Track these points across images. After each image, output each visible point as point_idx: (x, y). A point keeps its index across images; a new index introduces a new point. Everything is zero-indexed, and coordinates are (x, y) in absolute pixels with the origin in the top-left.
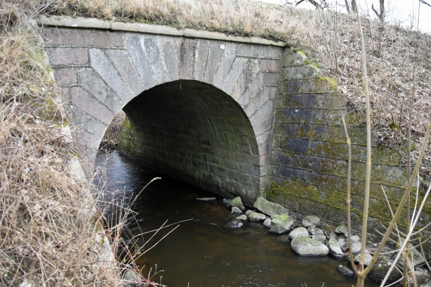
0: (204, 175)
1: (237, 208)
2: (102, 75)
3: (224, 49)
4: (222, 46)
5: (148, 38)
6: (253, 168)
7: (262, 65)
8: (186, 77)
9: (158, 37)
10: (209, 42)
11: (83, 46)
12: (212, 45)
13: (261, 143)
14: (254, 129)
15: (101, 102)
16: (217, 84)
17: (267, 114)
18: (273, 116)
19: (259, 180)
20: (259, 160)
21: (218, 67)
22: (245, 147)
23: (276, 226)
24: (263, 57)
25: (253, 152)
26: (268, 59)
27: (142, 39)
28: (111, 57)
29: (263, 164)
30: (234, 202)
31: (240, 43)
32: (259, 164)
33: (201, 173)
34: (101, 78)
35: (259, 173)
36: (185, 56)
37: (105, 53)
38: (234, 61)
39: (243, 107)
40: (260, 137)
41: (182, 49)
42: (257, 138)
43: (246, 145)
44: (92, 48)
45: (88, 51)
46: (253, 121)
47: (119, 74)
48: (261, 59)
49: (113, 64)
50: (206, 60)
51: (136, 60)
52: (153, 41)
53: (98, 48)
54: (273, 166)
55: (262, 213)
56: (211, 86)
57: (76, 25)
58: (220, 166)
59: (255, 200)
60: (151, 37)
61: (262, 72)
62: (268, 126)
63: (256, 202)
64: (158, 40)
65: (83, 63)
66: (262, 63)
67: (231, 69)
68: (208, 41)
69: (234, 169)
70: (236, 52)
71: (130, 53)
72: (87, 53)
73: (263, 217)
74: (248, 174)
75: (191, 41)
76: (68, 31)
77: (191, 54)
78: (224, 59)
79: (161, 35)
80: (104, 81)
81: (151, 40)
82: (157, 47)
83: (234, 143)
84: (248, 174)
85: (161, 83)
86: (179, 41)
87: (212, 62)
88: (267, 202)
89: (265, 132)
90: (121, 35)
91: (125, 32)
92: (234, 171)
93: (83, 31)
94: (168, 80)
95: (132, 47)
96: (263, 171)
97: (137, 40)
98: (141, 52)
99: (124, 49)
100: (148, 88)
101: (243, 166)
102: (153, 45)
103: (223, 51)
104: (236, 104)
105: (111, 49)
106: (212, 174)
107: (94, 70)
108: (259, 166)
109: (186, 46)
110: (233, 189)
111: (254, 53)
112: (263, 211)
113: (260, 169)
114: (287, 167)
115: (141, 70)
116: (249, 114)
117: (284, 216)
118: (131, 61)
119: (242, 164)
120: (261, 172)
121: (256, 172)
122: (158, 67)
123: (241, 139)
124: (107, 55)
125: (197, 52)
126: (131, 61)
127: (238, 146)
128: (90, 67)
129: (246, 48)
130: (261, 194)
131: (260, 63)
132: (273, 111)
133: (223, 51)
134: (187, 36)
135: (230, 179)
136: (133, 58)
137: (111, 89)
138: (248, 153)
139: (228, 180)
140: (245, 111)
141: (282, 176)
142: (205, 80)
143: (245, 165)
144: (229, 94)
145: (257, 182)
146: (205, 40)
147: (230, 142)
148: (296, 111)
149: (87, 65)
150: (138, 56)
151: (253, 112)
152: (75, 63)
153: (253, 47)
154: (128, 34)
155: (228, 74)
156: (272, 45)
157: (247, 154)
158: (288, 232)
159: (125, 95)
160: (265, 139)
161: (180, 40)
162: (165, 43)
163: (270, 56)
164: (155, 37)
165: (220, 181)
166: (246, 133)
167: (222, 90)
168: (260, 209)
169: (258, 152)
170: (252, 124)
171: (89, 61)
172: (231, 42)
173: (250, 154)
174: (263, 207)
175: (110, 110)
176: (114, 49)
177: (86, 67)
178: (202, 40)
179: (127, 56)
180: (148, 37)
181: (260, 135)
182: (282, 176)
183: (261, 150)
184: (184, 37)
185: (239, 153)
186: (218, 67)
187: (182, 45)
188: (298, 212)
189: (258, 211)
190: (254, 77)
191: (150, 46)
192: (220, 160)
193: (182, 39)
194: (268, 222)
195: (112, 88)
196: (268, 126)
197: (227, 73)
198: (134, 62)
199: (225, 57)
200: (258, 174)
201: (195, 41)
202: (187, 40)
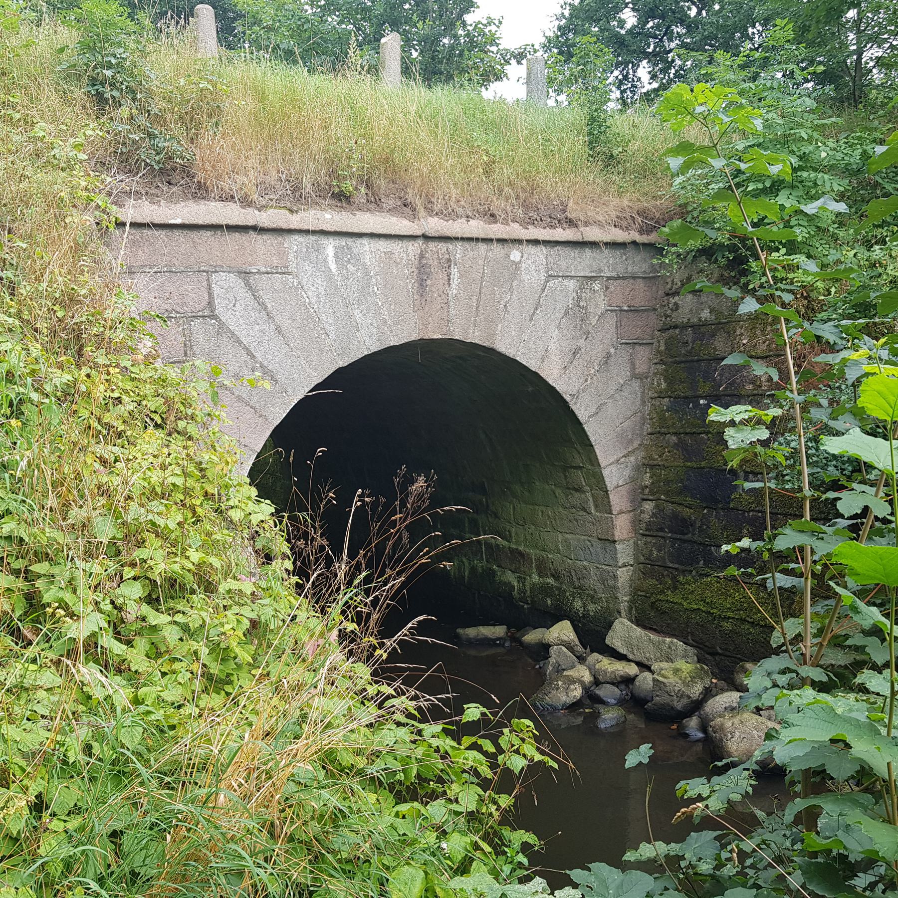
0: (473, 570)
1: (564, 649)
2: (241, 334)
3: (520, 262)
4: (515, 255)
5: (344, 243)
6: (598, 545)
7: (612, 293)
8: (434, 332)
9: (365, 241)
10: (483, 247)
11: (196, 268)
12: (490, 254)
13: (615, 483)
14: (597, 451)
15: (239, 399)
16: (503, 347)
17: (629, 413)
18: (643, 418)
19: (615, 577)
20: (613, 527)
21: (505, 306)
22: (577, 495)
23: (668, 689)
24: (614, 274)
25: (596, 506)
26: (624, 278)
27: (330, 246)
28: (261, 293)
29: (625, 536)
30: (556, 635)
31: (557, 243)
32: (613, 535)
33: (467, 564)
34: (240, 342)
35: (615, 559)
36: (429, 282)
37: (247, 284)
38: (543, 290)
39: (568, 398)
40: (614, 468)
41: (422, 272)
42: (606, 473)
43: (576, 490)
44: (216, 272)
45: (208, 280)
46: (592, 430)
47: (279, 330)
48: (609, 278)
49: (266, 308)
50: (478, 290)
51: (318, 296)
52: (355, 251)
53: (229, 272)
54: (649, 539)
55: (629, 660)
56: (491, 351)
57: (178, 221)
58: (514, 546)
59: (609, 625)
60: (349, 241)
61: (612, 311)
62: (631, 442)
63: (610, 633)
64: (367, 248)
65: (198, 307)
66: (612, 288)
67: (536, 309)
68: (480, 244)
69: (550, 551)
70: (548, 269)
71: (304, 282)
72: (205, 284)
73: (632, 669)
74: (585, 563)
75: (442, 246)
76: (162, 234)
77: (442, 276)
78: (519, 285)
79: (372, 235)
80: (246, 349)
81: (349, 248)
82: (364, 264)
83: (547, 487)
84: (585, 563)
85: (375, 348)
86: (414, 248)
87: (493, 293)
88: (639, 631)
89: (624, 456)
90: (280, 239)
91: (290, 231)
92: (550, 556)
93: (194, 235)
94: (395, 340)
95: (309, 268)
96: (624, 553)
97: (318, 250)
98: (330, 278)
99: (289, 273)
100: (343, 362)
101: (574, 543)
102: (356, 259)
103: (517, 265)
104: (553, 390)
105: (259, 272)
106: (495, 567)
107: (221, 323)
108: (614, 541)
109: (431, 260)
110: (549, 602)
111: (591, 266)
112: (631, 657)
113: (616, 548)
114: (685, 541)
115: (331, 321)
116: (582, 415)
117: (686, 667)
118: (307, 300)
119: (569, 536)
120: (619, 556)
121: (608, 557)
122: (368, 311)
123: (566, 476)
124: (250, 288)
125: (454, 271)
126: (307, 300)
127: (558, 491)
128: (213, 317)
129: (574, 253)
130: (623, 614)
131: (607, 288)
132: (643, 403)
133: (517, 265)
134: (433, 235)
135: (540, 576)
136: (310, 294)
137: (262, 366)
138: (584, 509)
139: (536, 578)
140: (573, 407)
141: (676, 566)
142: (475, 337)
143: (579, 540)
144: (533, 369)
145: (611, 582)
146: (473, 244)
147: (537, 484)
148: (702, 402)
149: (207, 313)
150: (322, 289)
151: (594, 410)
152: (178, 309)
153: (588, 252)
154: (296, 237)
155: (531, 320)
156: (634, 243)
157: (582, 513)
158: (696, 706)
159: (294, 380)
160: (627, 472)
161: (416, 245)
162: (383, 255)
163: (630, 269)
164: (359, 241)
165: (516, 584)
166: (578, 462)
167: (518, 359)
168: (623, 650)
169: (610, 506)
170: (592, 439)
171: (211, 304)
172: (536, 242)
173: (589, 513)
174: (629, 645)
175: (261, 416)
176: (268, 273)
177: (204, 317)
178: (467, 245)
179: (297, 289)
180: (343, 241)
181: (613, 463)
182: (676, 566)
183: (618, 500)
184: (426, 237)
185: (561, 509)
186: (505, 306)
187: (422, 256)
188: (720, 654)
189: (621, 657)
190: (594, 323)
191: (349, 262)
192: (513, 530)
193: (420, 242)
194: (646, 680)
195: (266, 363)
196: (631, 442)
197: (528, 318)
198: (313, 301)
199: (521, 281)
200: (612, 563)
201: (451, 247)
202: (432, 245)
